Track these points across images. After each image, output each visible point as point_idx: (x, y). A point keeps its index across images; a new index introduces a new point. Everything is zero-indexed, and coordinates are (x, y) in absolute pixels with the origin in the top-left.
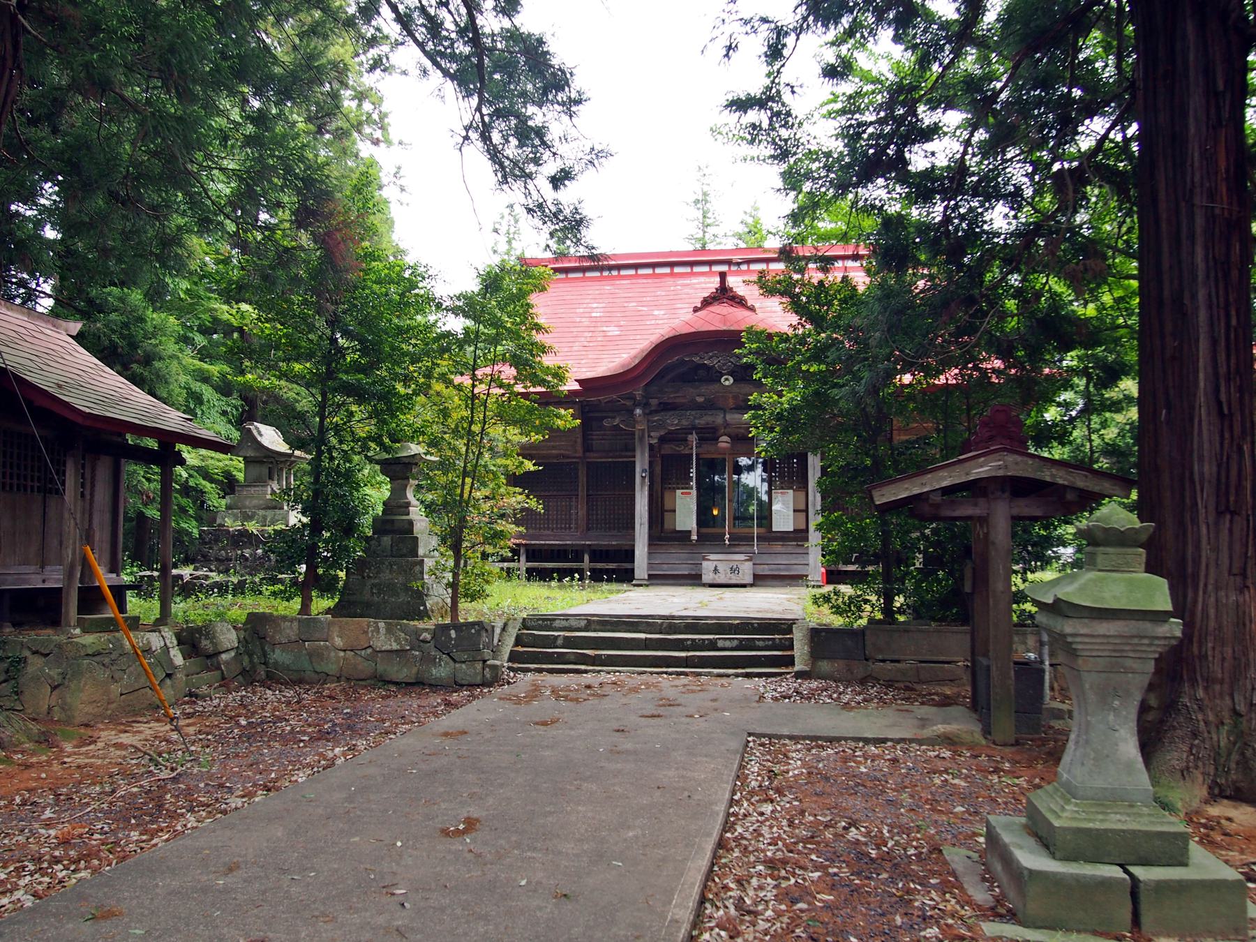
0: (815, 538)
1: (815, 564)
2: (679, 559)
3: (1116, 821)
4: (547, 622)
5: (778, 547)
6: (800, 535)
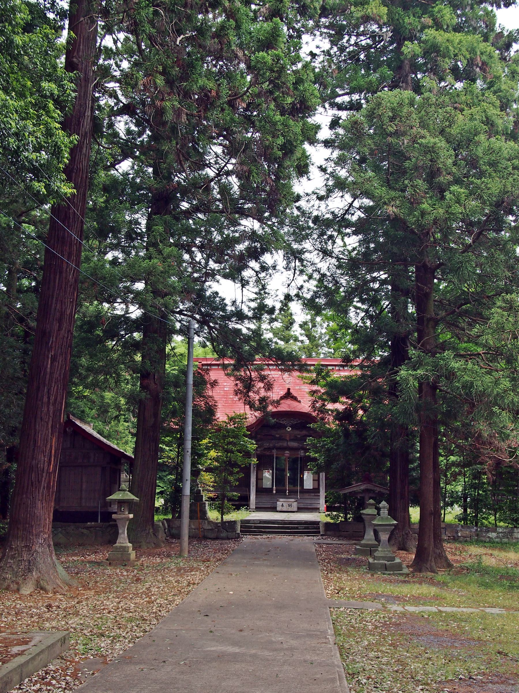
0: (323, 494)
1: (322, 504)
2: (268, 499)
3: (370, 542)
4: (248, 521)
5: (306, 496)
6: (316, 491)
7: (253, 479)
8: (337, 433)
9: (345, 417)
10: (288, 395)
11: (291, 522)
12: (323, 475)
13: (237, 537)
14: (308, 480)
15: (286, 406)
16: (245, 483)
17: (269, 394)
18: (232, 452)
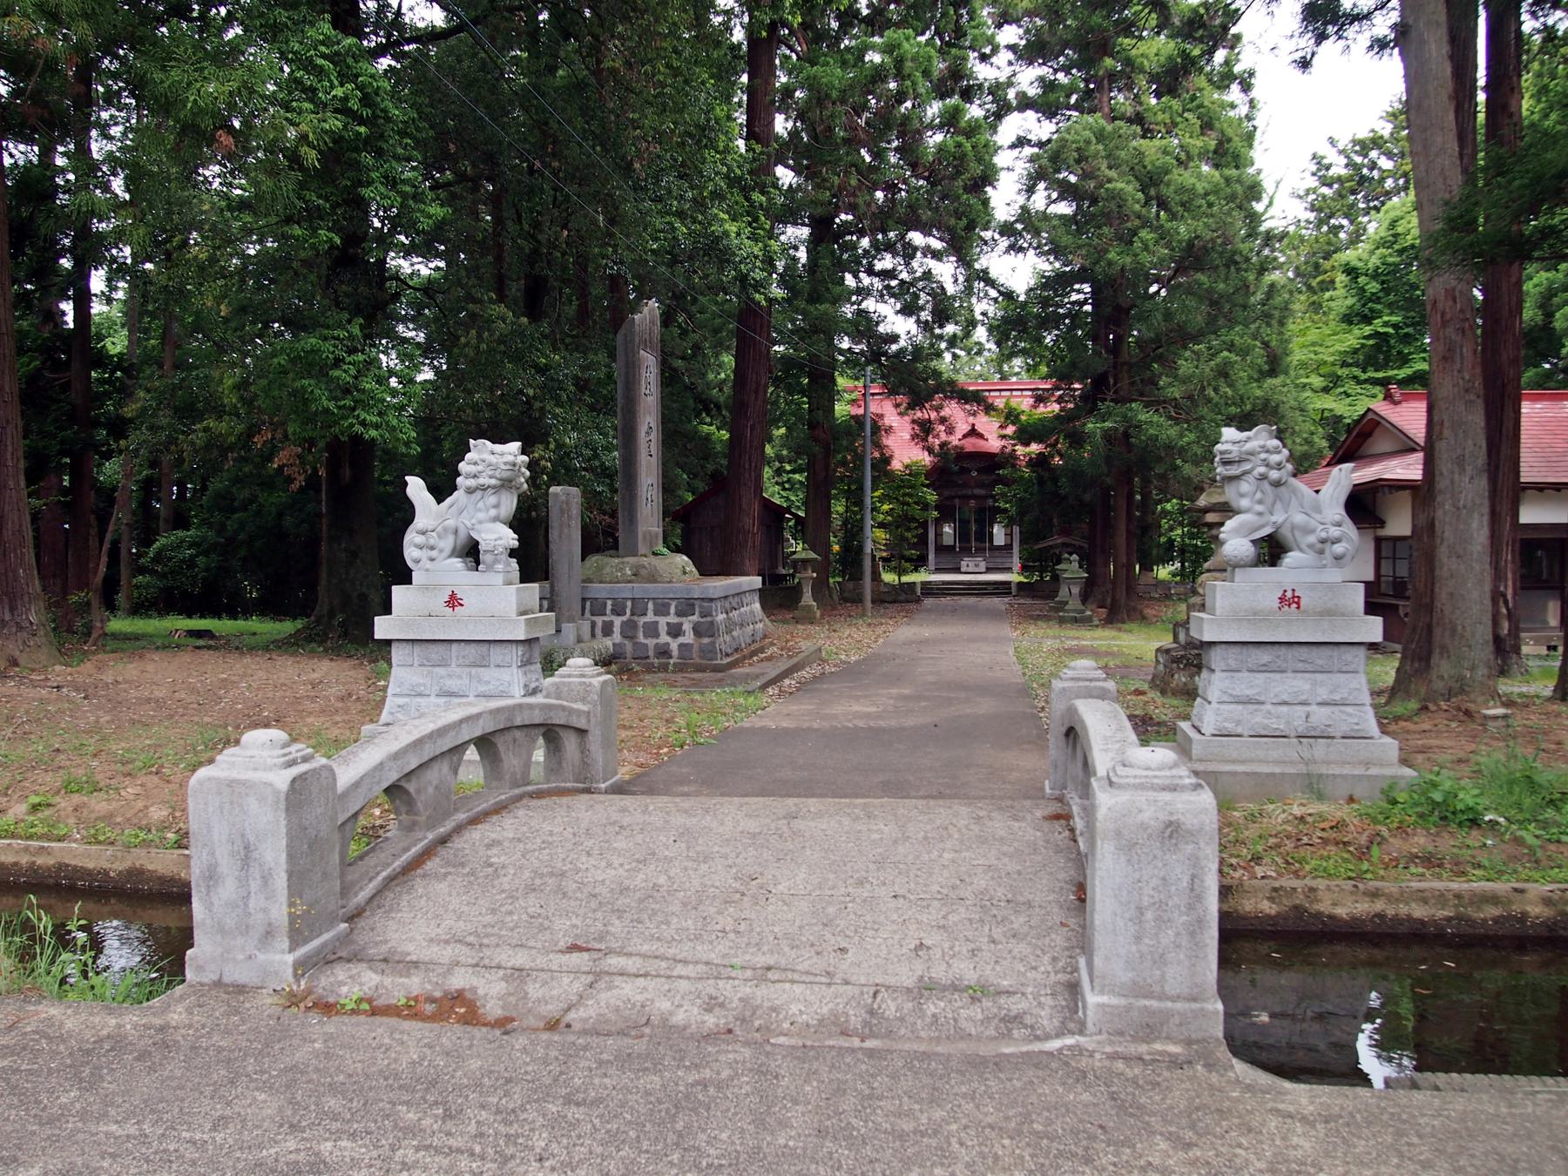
1: (1016, 563)
2: (949, 557)
5: (997, 553)
6: (1008, 547)
7: (931, 535)
8: (1030, 480)
9: (1039, 462)
10: (973, 432)
11: (979, 583)
12: (1016, 529)
13: (918, 601)
14: (999, 534)
15: (971, 445)
16: (923, 540)
17: (951, 438)
18: (908, 504)
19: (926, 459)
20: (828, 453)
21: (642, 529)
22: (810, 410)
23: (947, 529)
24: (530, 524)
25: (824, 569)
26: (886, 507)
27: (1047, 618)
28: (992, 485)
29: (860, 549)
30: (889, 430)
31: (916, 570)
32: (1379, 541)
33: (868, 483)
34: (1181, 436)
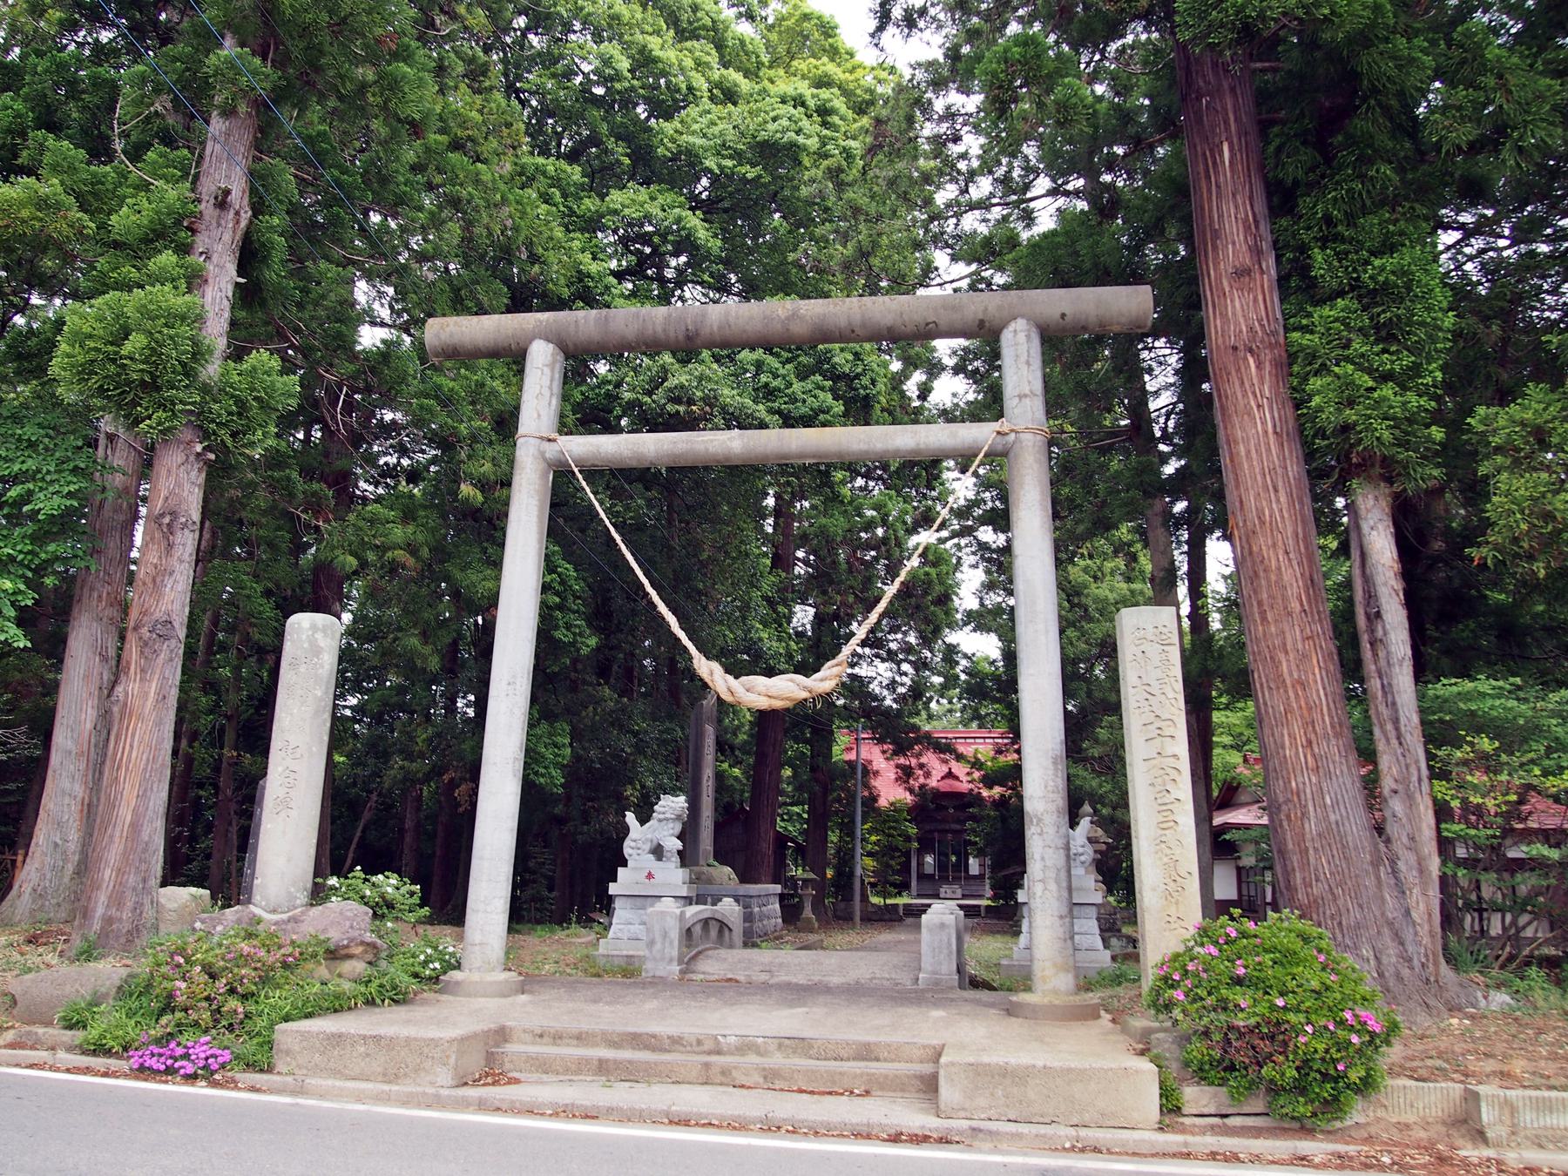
6: (981, 877)
13: (900, 920)
14: (974, 865)
15: (946, 786)
16: (906, 868)
19: (909, 798)
20: (826, 791)
21: (702, 847)
22: (812, 757)
23: (929, 859)
24: (688, 833)
25: (821, 885)
26: (873, 838)
27: (1005, 933)
28: (963, 822)
29: (852, 874)
30: (876, 773)
31: (900, 894)
32: (1239, 870)
33: (859, 818)
34: (1101, 786)
